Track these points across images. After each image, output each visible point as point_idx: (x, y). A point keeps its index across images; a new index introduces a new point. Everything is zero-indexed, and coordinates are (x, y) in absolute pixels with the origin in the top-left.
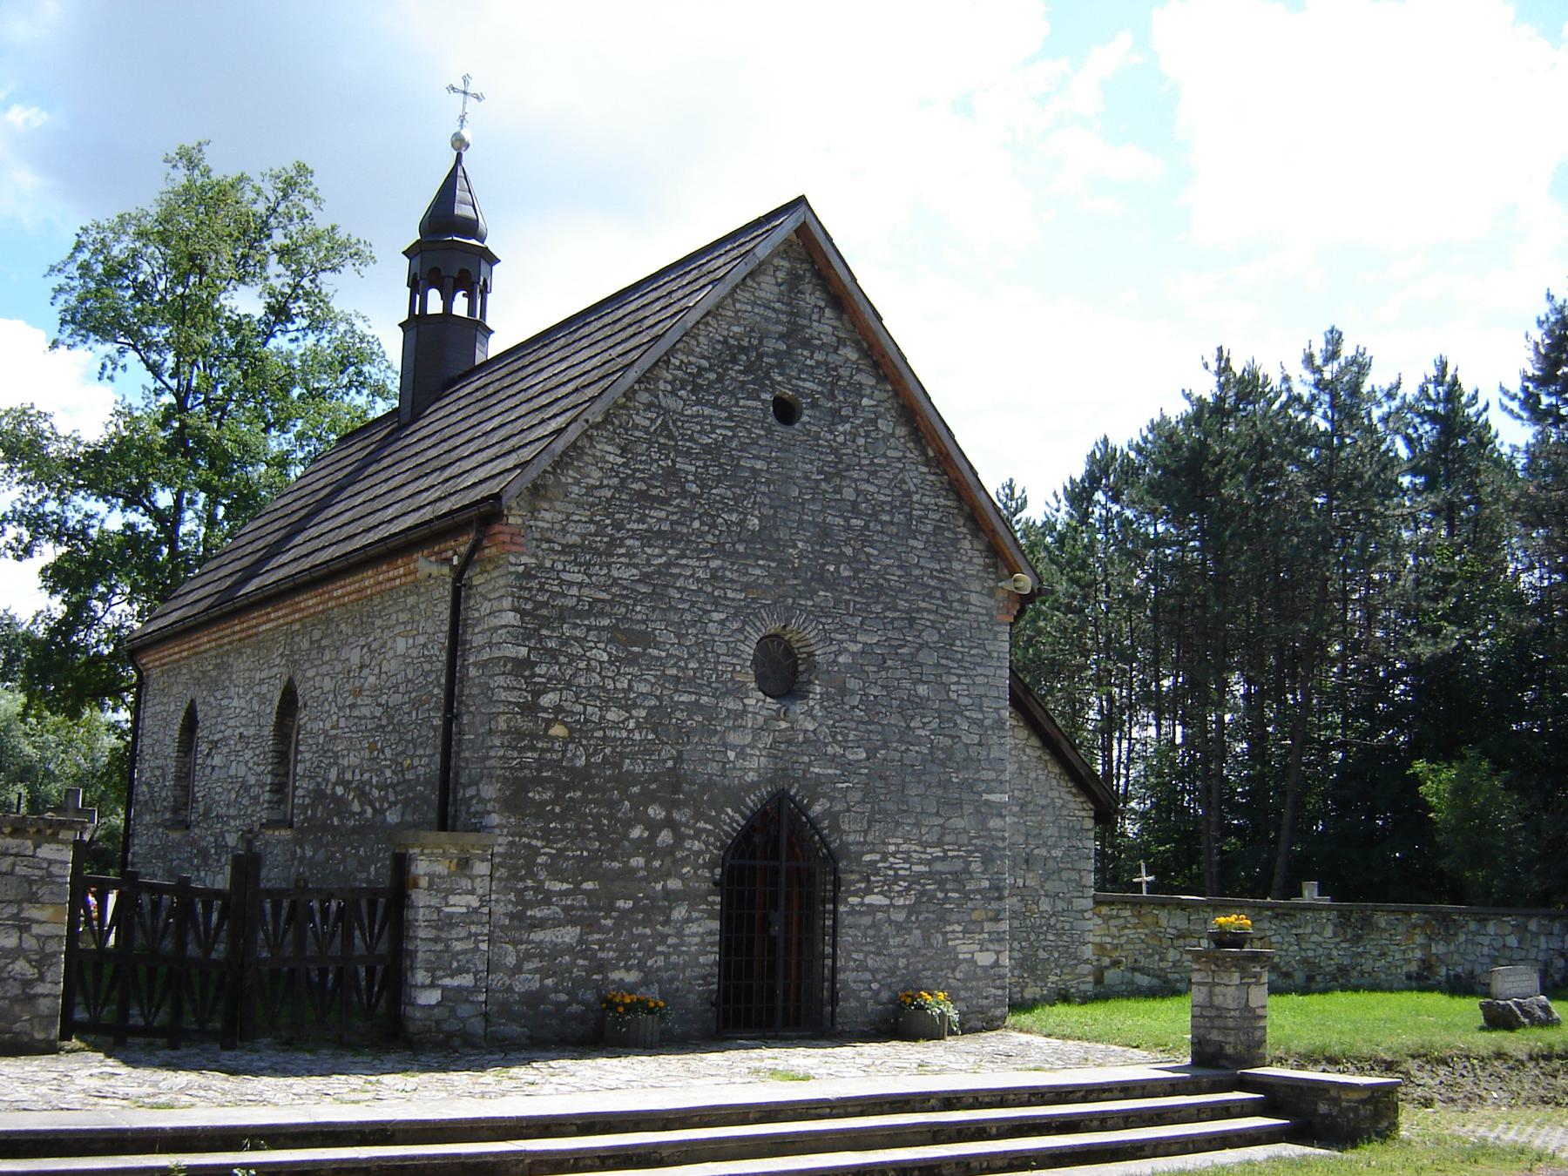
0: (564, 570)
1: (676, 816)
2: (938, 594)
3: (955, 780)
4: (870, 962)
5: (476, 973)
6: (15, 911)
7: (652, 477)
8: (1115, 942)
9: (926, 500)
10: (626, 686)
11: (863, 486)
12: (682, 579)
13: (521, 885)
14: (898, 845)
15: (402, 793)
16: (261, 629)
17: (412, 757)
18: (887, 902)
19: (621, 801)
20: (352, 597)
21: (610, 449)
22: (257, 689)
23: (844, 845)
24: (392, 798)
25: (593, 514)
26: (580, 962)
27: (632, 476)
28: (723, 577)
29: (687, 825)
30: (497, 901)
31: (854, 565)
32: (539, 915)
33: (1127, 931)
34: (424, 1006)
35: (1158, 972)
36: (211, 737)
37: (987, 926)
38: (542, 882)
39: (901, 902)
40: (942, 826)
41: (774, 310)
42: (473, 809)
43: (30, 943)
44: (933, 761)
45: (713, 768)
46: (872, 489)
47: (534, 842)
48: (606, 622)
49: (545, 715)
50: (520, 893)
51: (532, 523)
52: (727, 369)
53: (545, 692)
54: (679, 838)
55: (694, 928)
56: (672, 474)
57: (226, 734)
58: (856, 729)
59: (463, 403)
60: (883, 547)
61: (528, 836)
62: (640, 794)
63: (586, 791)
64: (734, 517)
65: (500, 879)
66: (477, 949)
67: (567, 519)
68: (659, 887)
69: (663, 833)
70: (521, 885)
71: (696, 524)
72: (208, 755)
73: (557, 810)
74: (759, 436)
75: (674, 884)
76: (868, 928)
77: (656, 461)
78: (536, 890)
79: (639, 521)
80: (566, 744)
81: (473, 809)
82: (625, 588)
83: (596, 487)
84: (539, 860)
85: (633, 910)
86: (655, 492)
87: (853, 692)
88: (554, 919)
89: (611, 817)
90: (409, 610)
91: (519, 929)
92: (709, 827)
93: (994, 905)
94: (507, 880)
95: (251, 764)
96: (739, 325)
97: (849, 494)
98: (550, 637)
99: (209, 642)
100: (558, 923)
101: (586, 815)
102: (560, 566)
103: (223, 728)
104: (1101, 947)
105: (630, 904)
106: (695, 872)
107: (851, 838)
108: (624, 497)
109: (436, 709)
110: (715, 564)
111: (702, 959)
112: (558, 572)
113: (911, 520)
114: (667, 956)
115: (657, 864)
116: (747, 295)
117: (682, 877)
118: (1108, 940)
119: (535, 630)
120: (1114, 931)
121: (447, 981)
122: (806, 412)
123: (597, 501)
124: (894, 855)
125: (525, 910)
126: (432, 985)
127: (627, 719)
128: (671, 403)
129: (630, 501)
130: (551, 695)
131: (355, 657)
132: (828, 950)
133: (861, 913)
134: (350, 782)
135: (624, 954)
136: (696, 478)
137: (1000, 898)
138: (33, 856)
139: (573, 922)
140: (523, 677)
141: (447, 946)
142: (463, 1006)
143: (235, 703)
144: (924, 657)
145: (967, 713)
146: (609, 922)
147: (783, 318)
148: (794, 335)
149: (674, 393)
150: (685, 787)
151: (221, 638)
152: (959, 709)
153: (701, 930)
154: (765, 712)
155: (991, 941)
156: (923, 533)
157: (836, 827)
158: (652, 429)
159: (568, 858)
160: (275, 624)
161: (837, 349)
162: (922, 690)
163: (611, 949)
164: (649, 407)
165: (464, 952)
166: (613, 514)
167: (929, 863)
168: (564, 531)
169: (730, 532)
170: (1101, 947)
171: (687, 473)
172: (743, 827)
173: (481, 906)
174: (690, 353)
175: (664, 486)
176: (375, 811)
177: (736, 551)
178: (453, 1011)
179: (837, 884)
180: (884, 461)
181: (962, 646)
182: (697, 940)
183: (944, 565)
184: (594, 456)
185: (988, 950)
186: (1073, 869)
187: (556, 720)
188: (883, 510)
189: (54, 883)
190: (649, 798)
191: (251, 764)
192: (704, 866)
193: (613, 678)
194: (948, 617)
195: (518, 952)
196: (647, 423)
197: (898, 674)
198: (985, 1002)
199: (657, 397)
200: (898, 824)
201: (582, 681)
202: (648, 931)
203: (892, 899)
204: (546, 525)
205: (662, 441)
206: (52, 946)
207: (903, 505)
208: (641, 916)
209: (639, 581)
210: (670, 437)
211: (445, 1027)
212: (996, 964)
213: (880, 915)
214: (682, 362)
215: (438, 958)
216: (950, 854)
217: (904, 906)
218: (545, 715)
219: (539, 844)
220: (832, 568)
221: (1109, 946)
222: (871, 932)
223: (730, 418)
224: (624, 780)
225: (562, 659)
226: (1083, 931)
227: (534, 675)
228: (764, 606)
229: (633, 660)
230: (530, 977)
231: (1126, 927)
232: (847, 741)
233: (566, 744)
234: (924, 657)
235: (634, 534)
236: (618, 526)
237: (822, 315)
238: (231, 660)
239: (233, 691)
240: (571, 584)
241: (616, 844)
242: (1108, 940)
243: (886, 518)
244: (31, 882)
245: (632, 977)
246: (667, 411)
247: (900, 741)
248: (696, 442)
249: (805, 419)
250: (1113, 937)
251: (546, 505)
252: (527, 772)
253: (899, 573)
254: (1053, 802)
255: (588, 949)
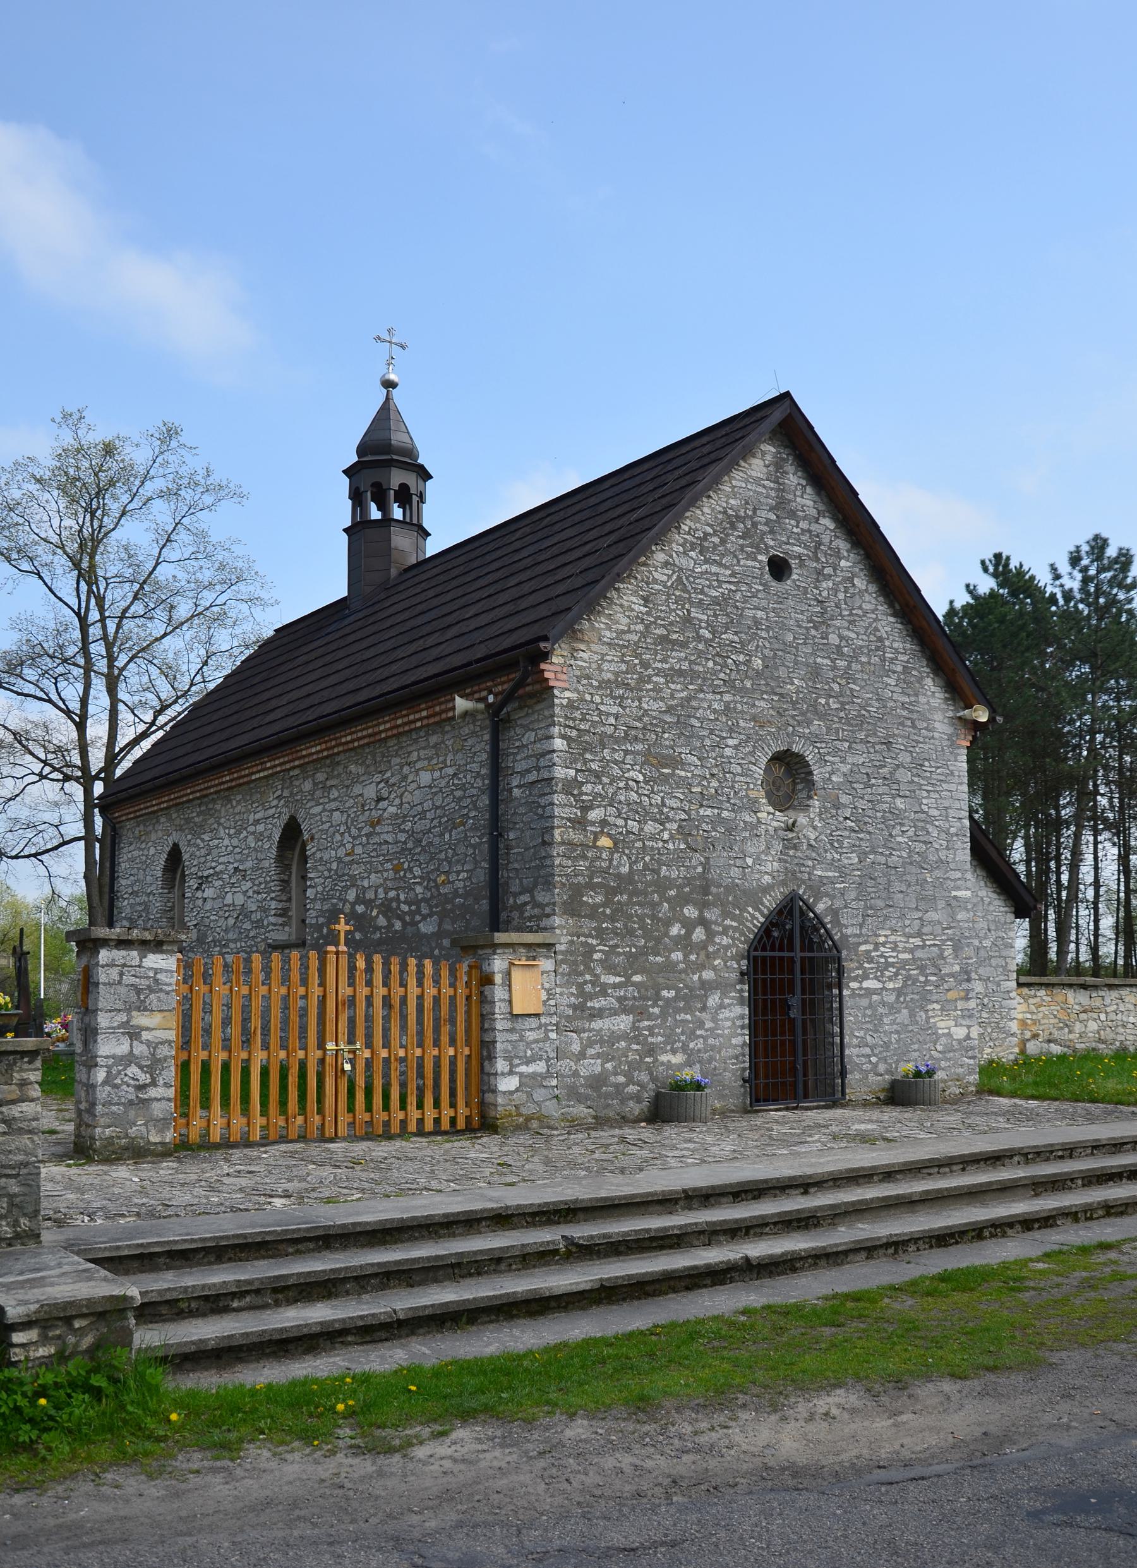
0: (602, 703)
1: (707, 915)
2: (909, 723)
3: (929, 880)
4: (869, 1038)
5: (548, 1059)
6: (125, 1019)
7: (671, 624)
8: (1034, 1017)
9: (896, 645)
10: (659, 802)
11: (846, 633)
12: (701, 711)
13: (580, 980)
14: (886, 936)
15: (437, 906)
16: (253, 777)
17: (447, 873)
18: (881, 986)
19: (661, 903)
20: (362, 742)
21: (634, 599)
22: (251, 829)
23: (845, 937)
24: (425, 911)
25: (623, 655)
26: (635, 1047)
27: (655, 623)
28: (735, 708)
29: (716, 923)
30: (561, 994)
31: (841, 699)
32: (597, 1006)
33: (1043, 1008)
34: (504, 1093)
35: (1068, 1043)
36: (200, 874)
37: (960, 1005)
38: (597, 976)
39: (891, 985)
40: (920, 919)
41: (764, 487)
42: (527, 914)
43: (140, 1049)
44: (911, 864)
45: (735, 872)
46: (853, 636)
47: (590, 941)
48: (639, 747)
49: (593, 829)
50: (580, 986)
51: (572, 662)
52: (727, 535)
53: (592, 808)
54: (710, 935)
55: (726, 1013)
56: (688, 620)
57: (217, 869)
58: (849, 837)
59: (424, 586)
60: (863, 683)
61: (586, 936)
62: (677, 896)
63: (631, 895)
64: (741, 658)
65: (562, 974)
66: (547, 1038)
67: (602, 659)
68: (696, 977)
69: (697, 930)
70: (580, 980)
71: (710, 664)
72: (197, 889)
73: (608, 911)
74: (758, 591)
75: (708, 975)
76: (866, 1008)
77: (674, 610)
78: (593, 983)
79: (661, 661)
80: (612, 854)
81: (527, 914)
82: (655, 718)
83: (623, 632)
84: (595, 957)
85: (676, 998)
86: (675, 636)
87: (845, 806)
88: (610, 1009)
89: (653, 917)
90: (433, 747)
91: (582, 1018)
92: (735, 924)
93: (965, 986)
94: (569, 975)
95: (250, 893)
96: (736, 498)
97: (834, 639)
98: (592, 761)
99: (192, 793)
100: (614, 1013)
101: (631, 916)
102: (597, 699)
103: (214, 864)
104: (1023, 1023)
105: (673, 993)
106: (725, 965)
107: (849, 931)
108: (649, 640)
109: (474, 828)
110: (728, 697)
111: (734, 1041)
112: (597, 704)
113: (884, 660)
114: (705, 1038)
115: (693, 957)
116: (741, 474)
117: (714, 969)
118: (1029, 1016)
119: (579, 754)
120: (1033, 1008)
121: (523, 1069)
122: (795, 571)
123: (626, 643)
124: (884, 944)
125: (586, 1001)
126: (511, 1073)
127: (662, 831)
128: (684, 562)
129: (654, 644)
130: (597, 811)
131: (370, 792)
132: (837, 1029)
133: (860, 996)
134: (371, 901)
135: (670, 1039)
136: (709, 625)
137: (969, 980)
138: (139, 966)
139: (626, 1011)
140: (572, 795)
141: (522, 1036)
142: (539, 1091)
143: (226, 842)
144: (900, 774)
145: (937, 823)
146: (656, 1010)
147: (772, 493)
148: (782, 506)
149: (685, 553)
150: (713, 890)
151: (206, 788)
152: (929, 819)
153: (732, 1015)
154: (775, 824)
155: (963, 1017)
156: (894, 672)
157: (836, 922)
158: (669, 584)
159: (619, 954)
160: (270, 772)
161: (818, 519)
162: (900, 803)
163: (659, 1034)
164: (666, 564)
165: (537, 1041)
166: (641, 654)
167: (911, 951)
168: (599, 668)
169: (738, 671)
170: (1023, 1023)
171: (700, 621)
172: (762, 924)
173: (549, 999)
174: (698, 520)
175: (682, 631)
176: (405, 924)
177: (744, 687)
178: (530, 1095)
179: (840, 971)
180: (860, 612)
181: (931, 766)
182: (729, 1024)
183: (913, 699)
184: (622, 606)
185: (961, 1025)
186: (1000, 957)
187: (602, 832)
188: (862, 653)
189: (161, 990)
190: (684, 900)
191: (250, 893)
192: (732, 958)
193: (648, 796)
194: (917, 742)
195: (581, 1039)
196: (665, 578)
197: (881, 790)
198: (961, 1070)
199: (671, 557)
200: (886, 918)
201: (623, 798)
202: (689, 1017)
203: (884, 983)
204: (584, 664)
205: (677, 593)
206: (164, 1051)
207: (877, 649)
208: (682, 1004)
209: (665, 712)
210: (685, 590)
211: (524, 1111)
212: (968, 1037)
213: (875, 997)
214: (690, 528)
215: (514, 1047)
216: (928, 943)
217: (894, 989)
218: (593, 829)
219: (594, 942)
220: (823, 701)
221: (1029, 1022)
222: (869, 1012)
223: (733, 574)
224: (662, 885)
225: (605, 780)
226: (1010, 1009)
227: (581, 794)
228: (769, 733)
229: (665, 779)
230: (593, 1061)
231: (1042, 1005)
232: (842, 848)
233: (612, 854)
234: (900, 774)
235: (659, 672)
236: (645, 665)
237: (804, 492)
238: (218, 807)
239: (222, 832)
240: (608, 714)
241: (658, 940)
242: (1029, 1016)
243: (864, 659)
244: (138, 991)
245: (677, 1059)
246: (681, 569)
247: (884, 846)
248: (706, 595)
249: (794, 577)
250: (1032, 1013)
251: (583, 647)
252: (580, 878)
253: (877, 705)
254: (982, 900)
255: (640, 1035)
